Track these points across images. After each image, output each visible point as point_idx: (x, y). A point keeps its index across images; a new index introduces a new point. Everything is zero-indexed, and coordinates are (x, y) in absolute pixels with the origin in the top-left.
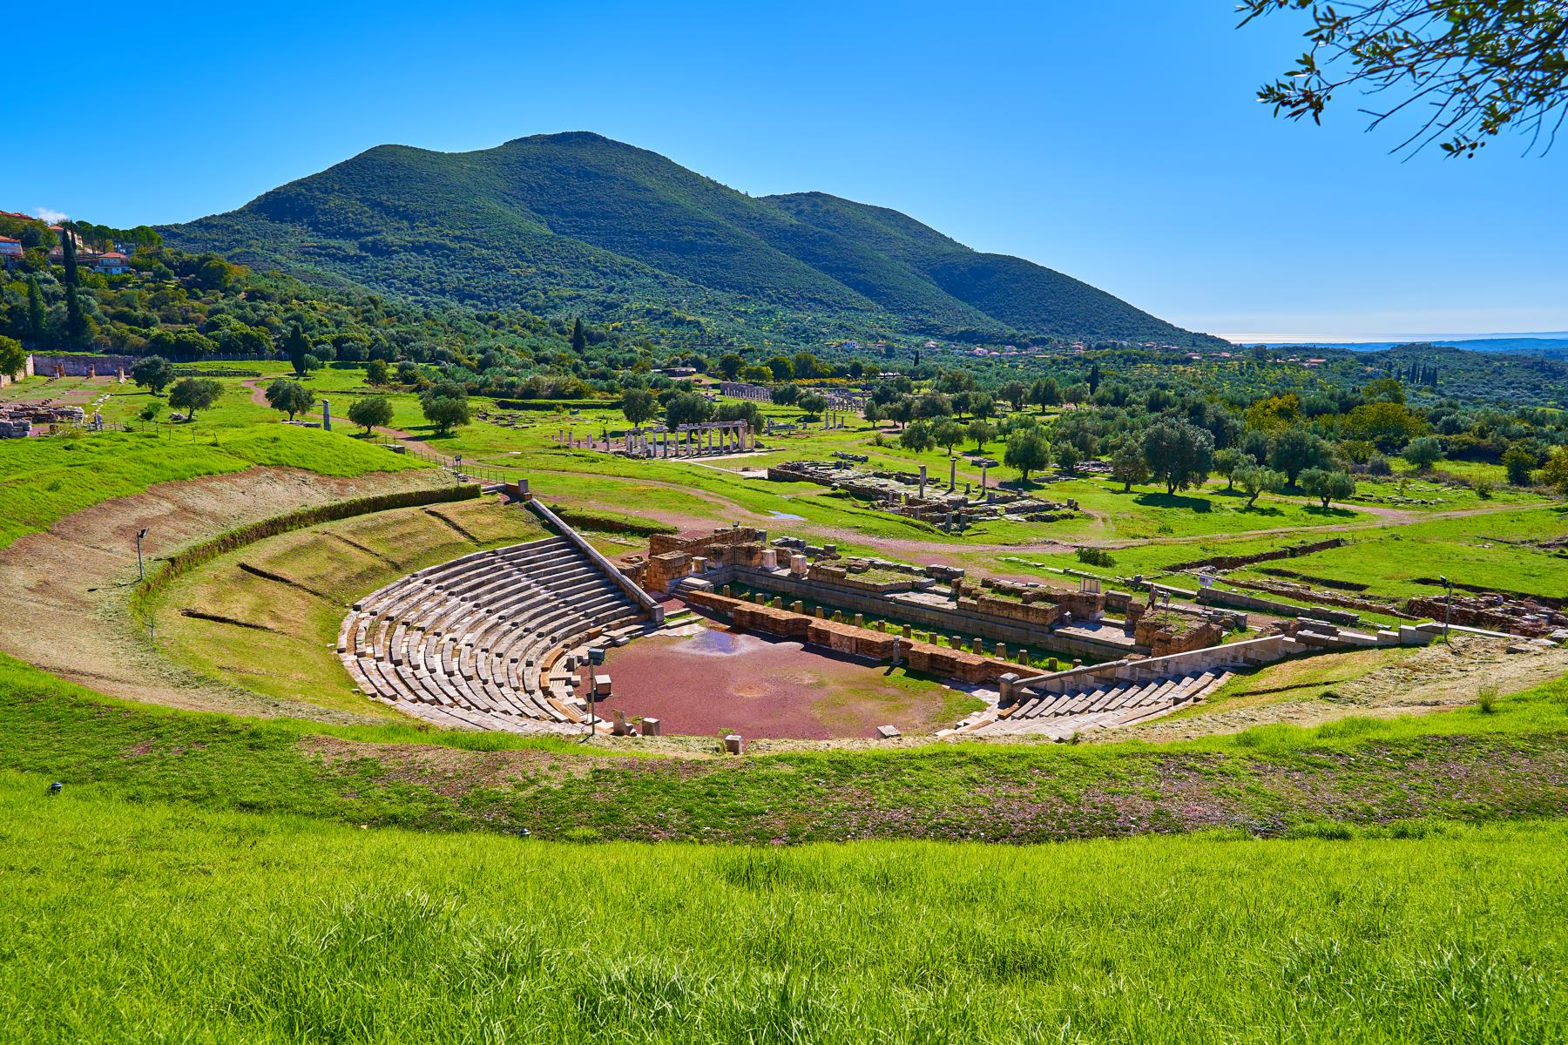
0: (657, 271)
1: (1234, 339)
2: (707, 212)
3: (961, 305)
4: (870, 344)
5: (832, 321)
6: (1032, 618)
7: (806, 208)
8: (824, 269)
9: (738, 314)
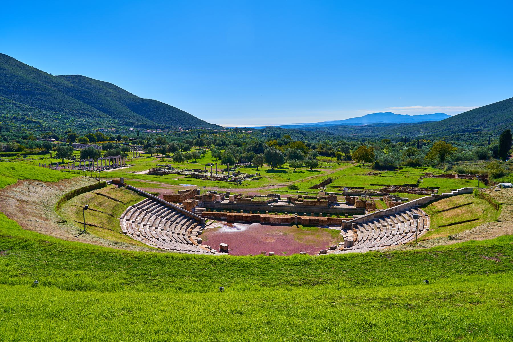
0: (15, 102)
1: (224, 126)
2: (34, 80)
3: (139, 116)
4: (109, 129)
5: (94, 121)
6: (322, 204)
7: (77, 81)
8: (87, 103)
9: (54, 119)
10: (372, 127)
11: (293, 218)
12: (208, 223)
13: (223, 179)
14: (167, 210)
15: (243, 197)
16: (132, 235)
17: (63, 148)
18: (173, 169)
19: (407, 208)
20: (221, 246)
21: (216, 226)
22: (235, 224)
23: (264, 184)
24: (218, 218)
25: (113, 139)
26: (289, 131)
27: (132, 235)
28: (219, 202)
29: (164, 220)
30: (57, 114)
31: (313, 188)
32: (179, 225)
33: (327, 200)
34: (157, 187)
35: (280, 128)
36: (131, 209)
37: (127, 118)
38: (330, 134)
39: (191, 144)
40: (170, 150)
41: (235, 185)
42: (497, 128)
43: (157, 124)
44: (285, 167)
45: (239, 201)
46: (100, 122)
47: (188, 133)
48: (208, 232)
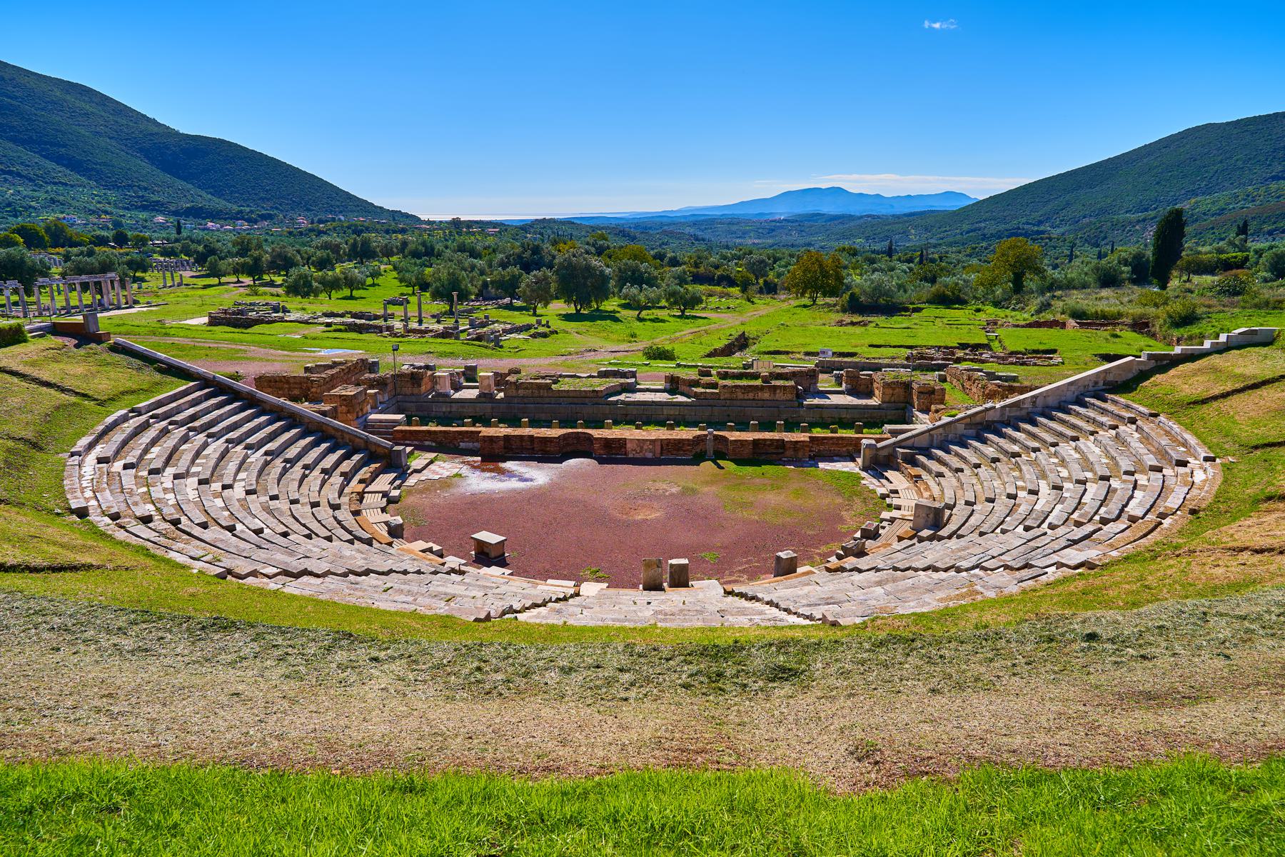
1: (423, 217)
3: (180, 184)
4: (93, 219)
6: (780, 396)
8: (14, 140)
10: (801, 223)
11: (698, 439)
12: (416, 463)
13: (445, 335)
14: (270, 423)
15: (524, 377)
16: (115, 517)
18: (285, 310)
19: (1070, 396)
20: (481, 545)
21: (446, 474)
22: (509, 465)
23: (569, 351)
24: (447, 446)
26: (594, 229)
27: (115, 517)
28: (447, 395)
29: (257, 457)
31: (710, 355)
32: (316, 472)
33: (792, 383)
34: (232, 357)
35: (569, 222)
36: (125, 419)
37: (146, 189)
38: (697, 239)
41: (483, 350)
42: (1080, 229)
43: (235, 208)
44: (610, 308)
45: (513, 392)
46: (61, 198)
48: (421, 492)
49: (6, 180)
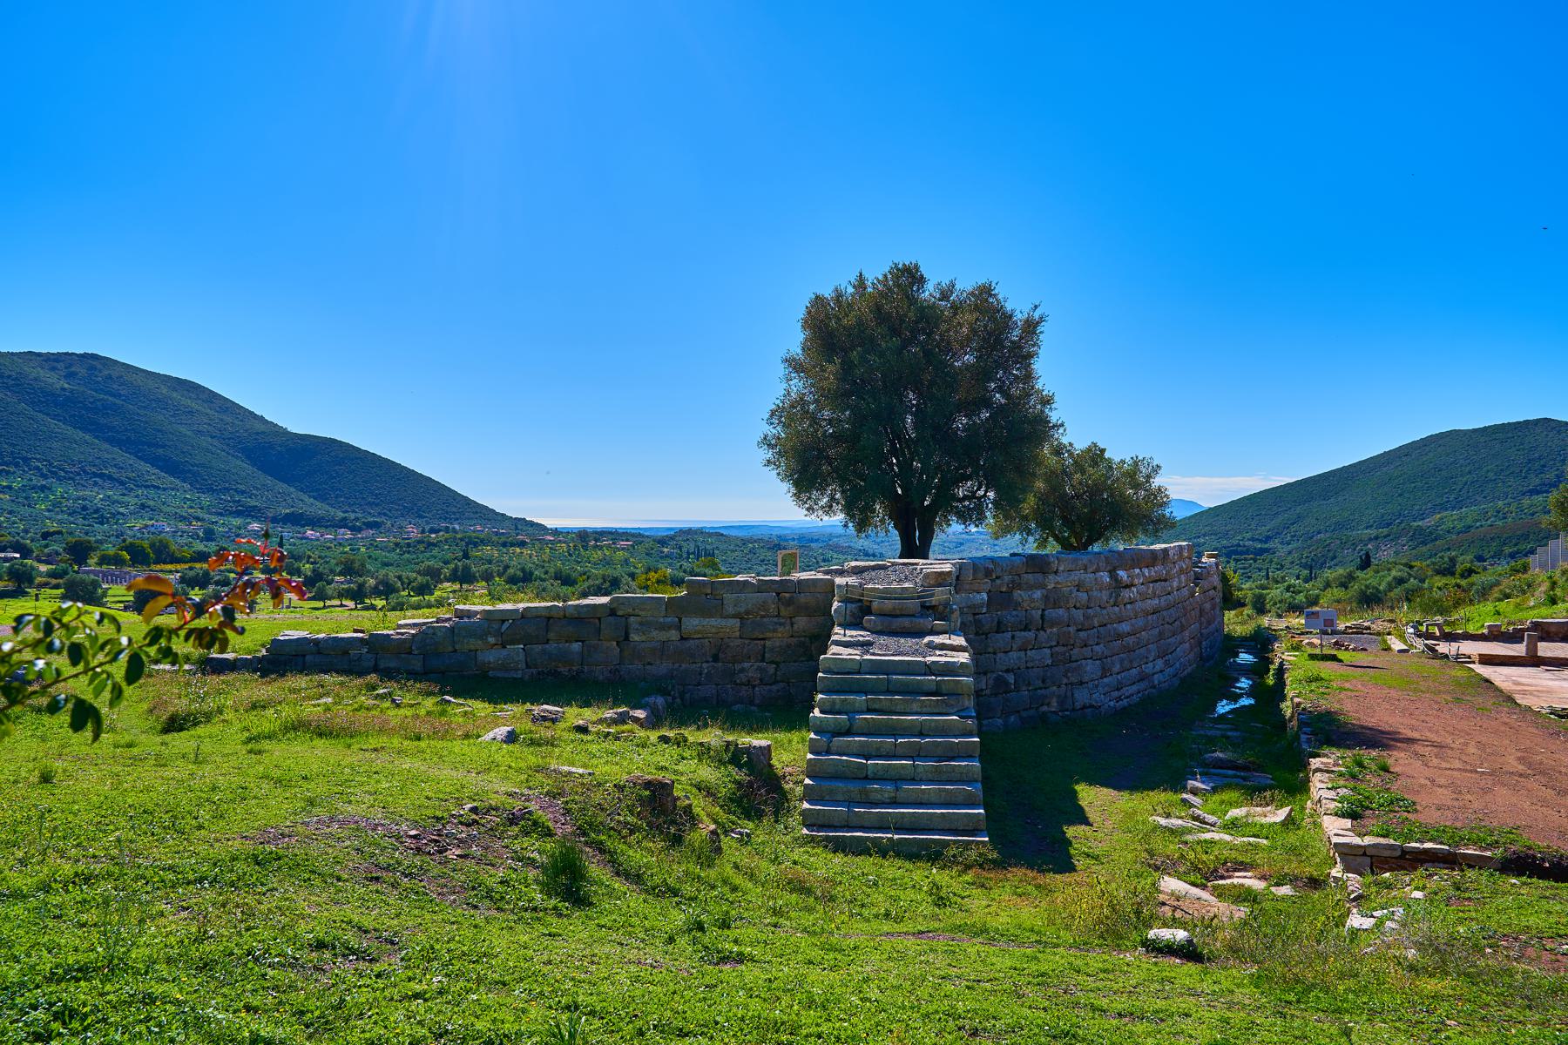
1: (550, 523)
3: (281, 487)
4: (182, 526)
7: (82, 372)
8: (112, 441)
17: (83, 582)
25: (202, 557)
26: (745, 542)
30: (8, 473)
37: (243, 492)
39: (435, 576)
40: (376, 592)
43: (340, 515)
46: (151, 503)
47: (434, 545)
49: (96, 484)
